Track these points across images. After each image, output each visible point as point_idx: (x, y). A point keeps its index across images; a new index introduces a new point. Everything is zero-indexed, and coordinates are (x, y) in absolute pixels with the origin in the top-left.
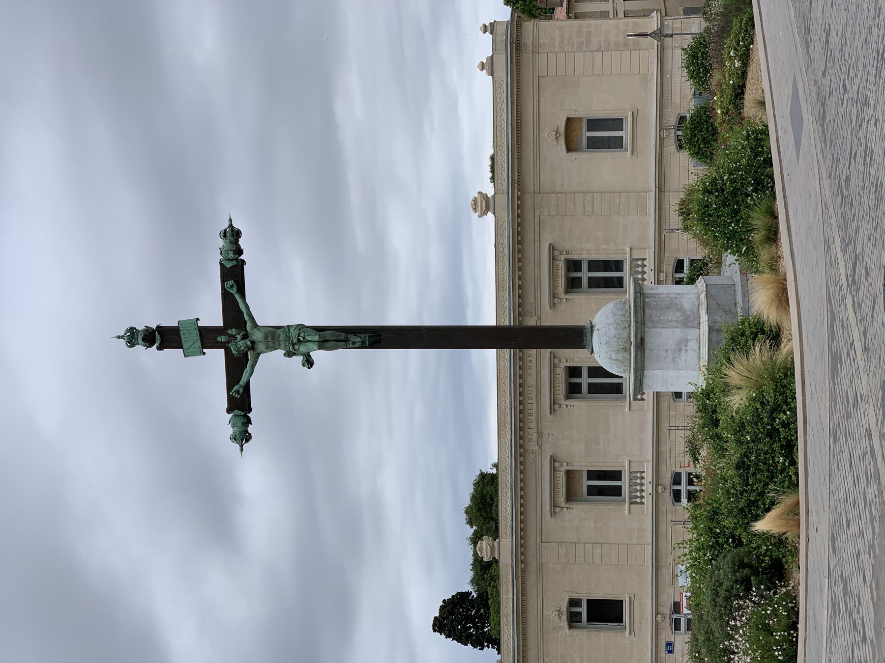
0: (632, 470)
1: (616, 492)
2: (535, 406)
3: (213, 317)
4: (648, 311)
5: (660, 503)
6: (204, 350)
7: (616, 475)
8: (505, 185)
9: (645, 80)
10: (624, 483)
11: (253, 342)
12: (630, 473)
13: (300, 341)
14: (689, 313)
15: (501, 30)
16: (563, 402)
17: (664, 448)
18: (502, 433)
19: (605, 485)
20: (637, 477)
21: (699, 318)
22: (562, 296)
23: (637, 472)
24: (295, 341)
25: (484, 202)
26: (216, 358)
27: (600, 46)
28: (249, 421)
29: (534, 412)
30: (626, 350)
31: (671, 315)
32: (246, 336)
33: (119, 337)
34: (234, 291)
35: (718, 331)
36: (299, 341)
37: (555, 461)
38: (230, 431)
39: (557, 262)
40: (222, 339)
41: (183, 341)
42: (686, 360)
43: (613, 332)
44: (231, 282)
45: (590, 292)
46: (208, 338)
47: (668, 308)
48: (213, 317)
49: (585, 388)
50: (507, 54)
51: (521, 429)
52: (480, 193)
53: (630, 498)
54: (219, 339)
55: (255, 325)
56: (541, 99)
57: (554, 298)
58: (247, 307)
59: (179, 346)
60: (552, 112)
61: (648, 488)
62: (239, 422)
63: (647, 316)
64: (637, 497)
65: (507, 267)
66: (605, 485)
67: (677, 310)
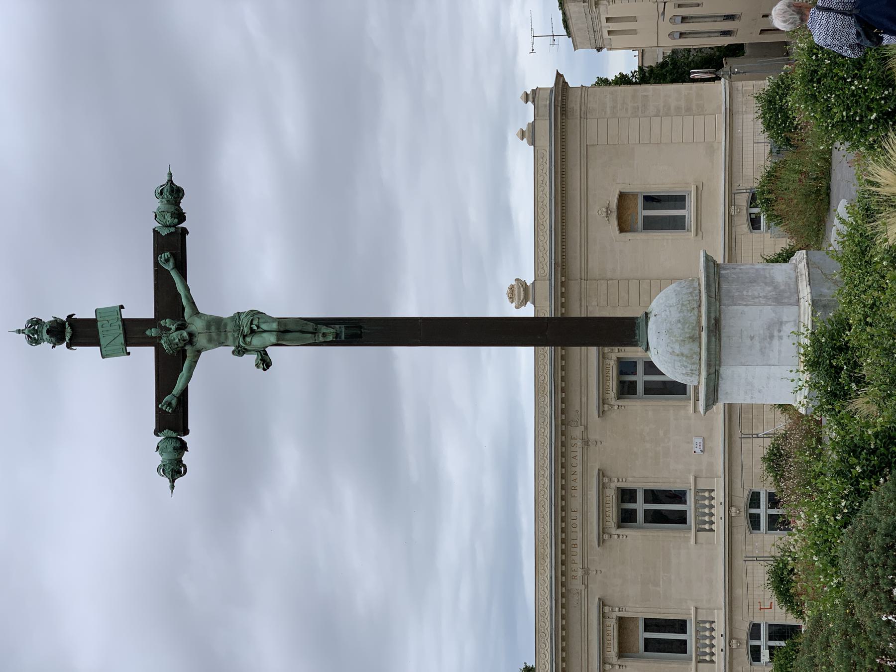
0: (700, 619)
1: (681, 647)
2: (580, 535)
3: (142, 306)
4: (724, 286)
5: (735, 662)
6: (129, 349)
7: (681, 626)
8: (547, 270)
9: (711, 150)
10: (690, 637)
11: (191, 335)
12: (697, 622)
13: (251, 334)
14: (782, 287)
15: (544, 101)
16: (614, 531)
17: (738, 592)
18: (541, 568)
19: (665, 508)
20: (705, 627)
21: (798, 292)
22: (613, 401)
23: (705, 622)
24: (246, 330)
25: (522, 290)
26: (144, 358)
27: (658, 111)
28: (183, 447)
29: (579, 542)
30: (696, 339)
31: (757, 290)
32: (182, 327)
33: (19, 331)
34: (169, 267)
35: (825, 307)
36: (252, 332)
37: (604, 605)
38: (158, 459)
39: (608, 361)
40: (152, 332)
41: (101, 336)
42: (780, 352)
43: (675, 315)
44: (166, 255)
45: (647, 528)
46: (134, 333)
47: (753, 281)
48: (142, 306)
49: (640, 516)
50: (550, 119)
51: (563, 563)
52: (517, 280)
53: (697, 655)
54: (148, 332)
55: (196, 312)
56: (590, 171)
57: (604, 404)
58: (187, 289)
59: (95, 342)
60: (602, 188)
61: (720, 642)
62: (170, 446)
63: (723, 291)
64: (705, 654)
65: (548, 367)
66: (665, 508)
67: (766, 284)
